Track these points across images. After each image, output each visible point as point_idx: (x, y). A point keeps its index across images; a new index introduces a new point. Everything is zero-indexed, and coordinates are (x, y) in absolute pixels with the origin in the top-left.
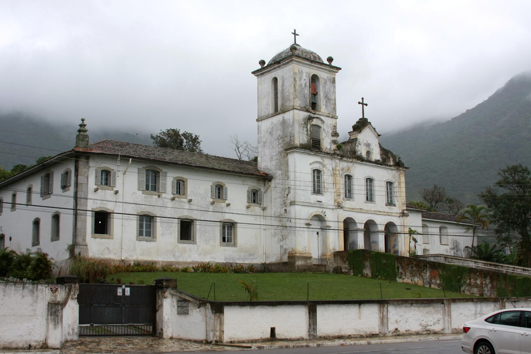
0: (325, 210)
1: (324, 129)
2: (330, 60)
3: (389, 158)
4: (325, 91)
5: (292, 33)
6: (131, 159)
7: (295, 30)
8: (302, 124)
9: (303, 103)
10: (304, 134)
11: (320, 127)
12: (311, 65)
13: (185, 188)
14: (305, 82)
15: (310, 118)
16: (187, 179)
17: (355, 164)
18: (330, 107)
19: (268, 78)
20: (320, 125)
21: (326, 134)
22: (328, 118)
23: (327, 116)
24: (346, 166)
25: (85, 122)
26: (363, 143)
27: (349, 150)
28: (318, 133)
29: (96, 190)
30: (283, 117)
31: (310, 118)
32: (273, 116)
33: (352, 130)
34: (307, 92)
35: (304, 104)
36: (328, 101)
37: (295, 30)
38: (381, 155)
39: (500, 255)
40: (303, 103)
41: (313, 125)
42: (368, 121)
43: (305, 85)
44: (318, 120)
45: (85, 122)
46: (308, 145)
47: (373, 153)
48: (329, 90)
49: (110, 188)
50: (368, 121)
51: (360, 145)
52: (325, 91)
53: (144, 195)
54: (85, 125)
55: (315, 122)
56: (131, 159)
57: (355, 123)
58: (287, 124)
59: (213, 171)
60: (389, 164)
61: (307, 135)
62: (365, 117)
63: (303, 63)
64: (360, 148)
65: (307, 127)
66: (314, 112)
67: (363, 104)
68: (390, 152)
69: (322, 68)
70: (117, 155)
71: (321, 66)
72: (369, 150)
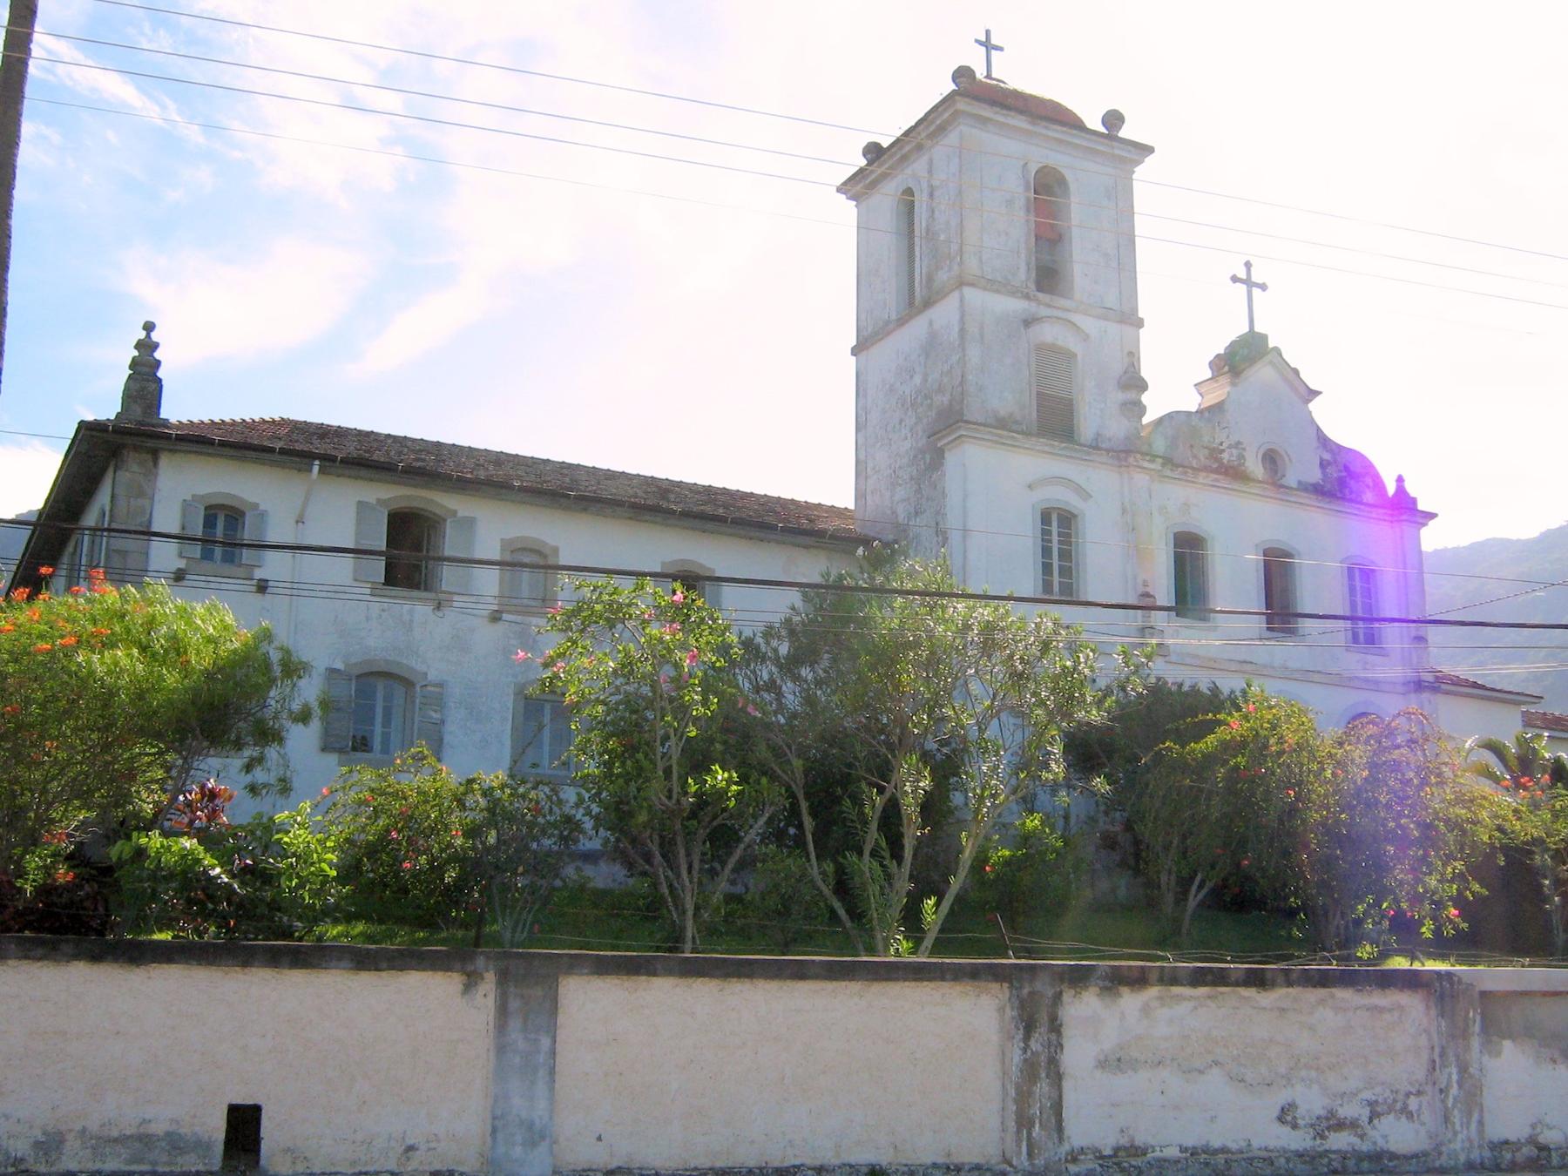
2: (1113, 119)
5: (977, 41)
7: (988, 33)
19: (890, 190)
25: (155, 336)
30: (931, 323)
32: (902, 322)
33: (1209, 374)
37: (988, 33)
42: (1271, 345)
45: (155, 336)
49: (241, 572)
50: (1271, 345)
57: (1140, 315)
58: (941, 344)
62: (1258, 329)
67: (1249, 283)
70: (280, 453)
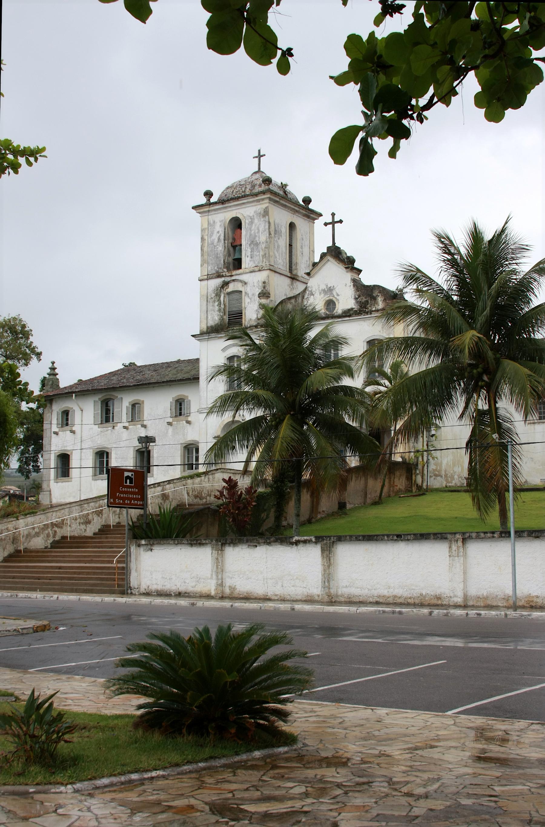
1: (246, 293)
3: (374, 299)
4: (251, 235)
6: (74, 395)
8: (212, 298)
10: (214, 311)
11: (241, 292)
13: (141, 412)
14: (218, 235)
15: (225, 284)
16: (143, 402)
20: (240, 289)
21: (251, 299)
22: (253, 274)
23: (251, 272)
26: (317, 291)
28: (240, 300)
29: (144, 426)
31: (225, 284)
35: (216, 268)
38: (356, 299)
39: (280, 459)
41: (229, 294)
43: (219, 239)
44: (236, 283)
46: (221, 325)
47: (338, 300)
48: (257, 231)
51: (313, 295)
53: (100, 429)
54: (55, 368)
55: (232, 287)
56: (74, 395)
59: (157, 385)
60: (374, 309)
61: (219, 310)
63: (215, 210)
64: (311, 300)
65: (219, 300)
66: (230, 274)
68: (379, 287)
69: (244, 203)
72: (331, 298)
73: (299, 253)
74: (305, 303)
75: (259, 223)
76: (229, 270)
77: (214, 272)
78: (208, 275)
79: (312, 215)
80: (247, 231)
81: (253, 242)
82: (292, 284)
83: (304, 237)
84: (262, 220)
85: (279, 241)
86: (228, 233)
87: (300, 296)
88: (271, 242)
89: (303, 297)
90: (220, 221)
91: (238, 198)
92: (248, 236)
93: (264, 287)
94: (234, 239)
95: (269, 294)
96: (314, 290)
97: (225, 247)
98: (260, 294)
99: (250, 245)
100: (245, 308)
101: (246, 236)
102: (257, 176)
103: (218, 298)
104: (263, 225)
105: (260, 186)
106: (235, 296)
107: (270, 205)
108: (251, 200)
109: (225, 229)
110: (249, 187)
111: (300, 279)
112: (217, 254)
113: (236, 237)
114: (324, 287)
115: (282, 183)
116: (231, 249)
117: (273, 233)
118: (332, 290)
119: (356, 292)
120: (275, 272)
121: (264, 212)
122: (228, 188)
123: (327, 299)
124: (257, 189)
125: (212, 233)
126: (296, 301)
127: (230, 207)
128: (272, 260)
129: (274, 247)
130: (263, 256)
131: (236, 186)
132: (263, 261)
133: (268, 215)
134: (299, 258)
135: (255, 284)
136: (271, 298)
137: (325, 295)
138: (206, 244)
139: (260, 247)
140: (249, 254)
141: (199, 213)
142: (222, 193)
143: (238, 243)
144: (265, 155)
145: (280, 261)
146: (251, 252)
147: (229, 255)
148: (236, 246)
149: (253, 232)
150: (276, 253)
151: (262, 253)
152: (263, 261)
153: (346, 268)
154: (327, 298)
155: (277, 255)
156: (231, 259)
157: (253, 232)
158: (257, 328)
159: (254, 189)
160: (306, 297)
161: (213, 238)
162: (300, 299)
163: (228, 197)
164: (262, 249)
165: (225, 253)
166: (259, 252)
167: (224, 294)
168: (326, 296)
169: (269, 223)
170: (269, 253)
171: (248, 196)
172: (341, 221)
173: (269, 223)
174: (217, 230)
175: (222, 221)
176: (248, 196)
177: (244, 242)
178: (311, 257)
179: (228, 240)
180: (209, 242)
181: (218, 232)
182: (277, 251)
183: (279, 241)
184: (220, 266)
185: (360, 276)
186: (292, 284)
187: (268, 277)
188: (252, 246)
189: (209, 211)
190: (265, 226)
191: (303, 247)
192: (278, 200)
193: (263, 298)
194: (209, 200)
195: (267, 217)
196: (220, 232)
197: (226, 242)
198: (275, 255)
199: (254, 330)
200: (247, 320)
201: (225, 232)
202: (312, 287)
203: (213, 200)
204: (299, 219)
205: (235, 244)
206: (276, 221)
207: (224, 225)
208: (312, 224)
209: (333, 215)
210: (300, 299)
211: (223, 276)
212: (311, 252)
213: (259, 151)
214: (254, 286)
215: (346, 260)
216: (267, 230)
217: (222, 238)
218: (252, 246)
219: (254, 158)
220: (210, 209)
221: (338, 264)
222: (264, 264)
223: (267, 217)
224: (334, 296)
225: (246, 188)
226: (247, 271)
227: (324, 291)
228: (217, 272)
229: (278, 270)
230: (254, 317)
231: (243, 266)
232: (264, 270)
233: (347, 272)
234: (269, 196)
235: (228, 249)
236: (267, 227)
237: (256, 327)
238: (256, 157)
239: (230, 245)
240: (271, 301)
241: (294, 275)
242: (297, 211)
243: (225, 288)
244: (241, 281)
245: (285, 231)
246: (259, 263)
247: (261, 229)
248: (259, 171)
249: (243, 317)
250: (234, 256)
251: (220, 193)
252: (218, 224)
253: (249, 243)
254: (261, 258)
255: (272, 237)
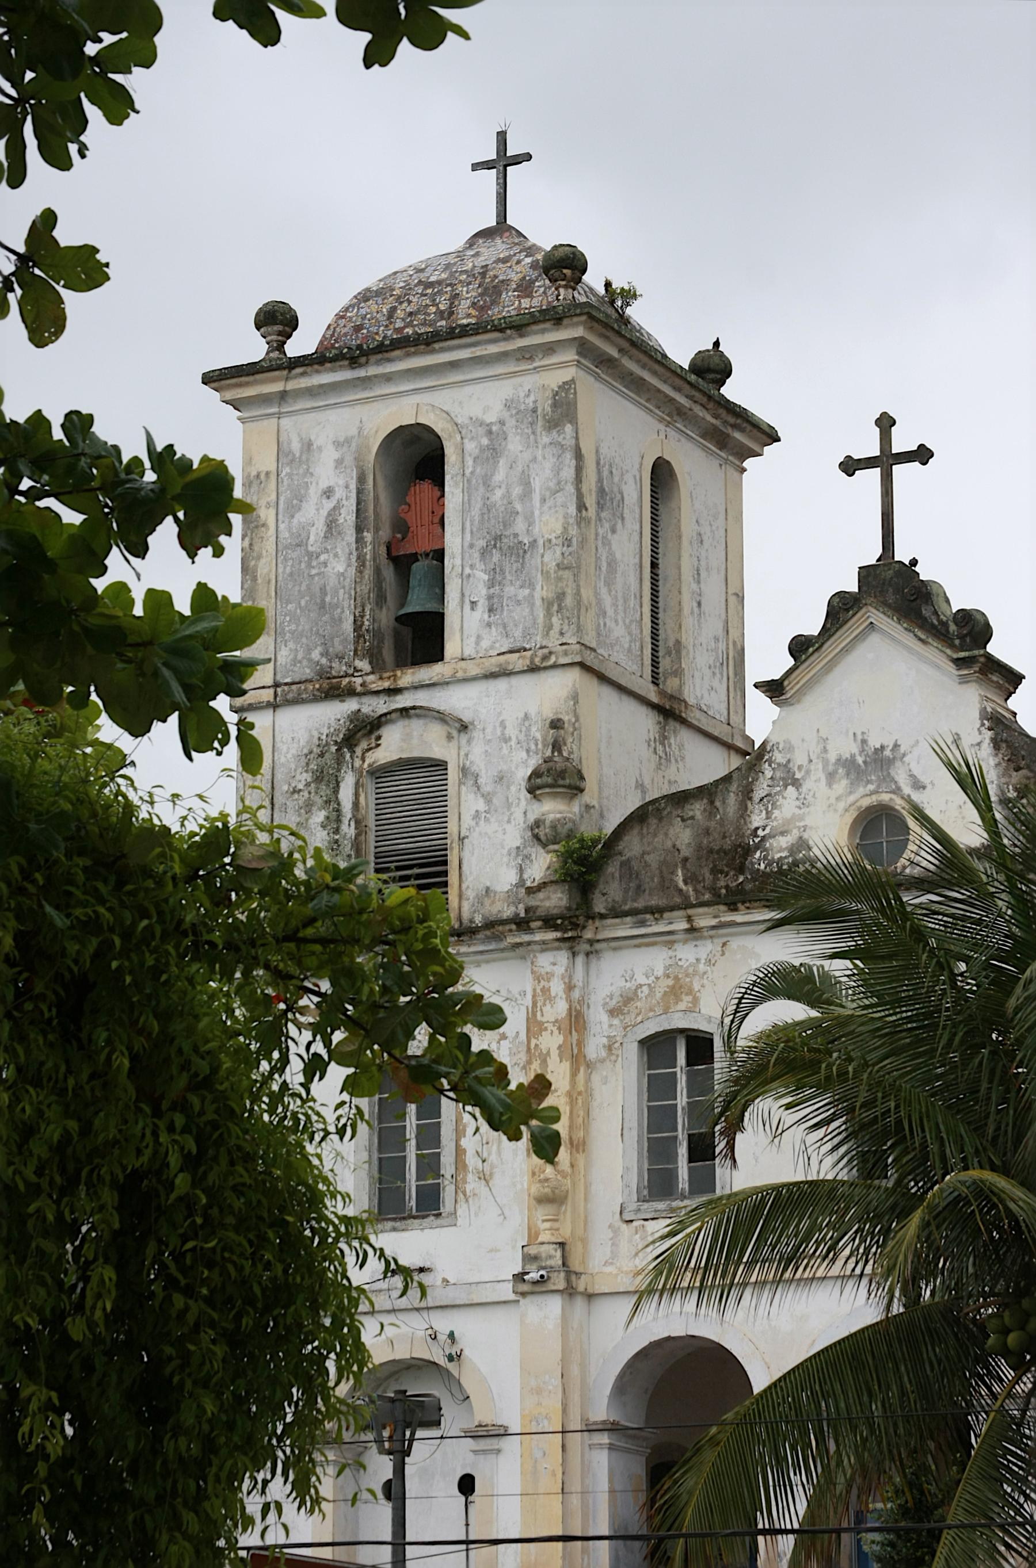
0: (443, 1323)
1: (464, 771)
4: (488, 507)
8: (296, 791)
9: (309, 650)
11: (439, 766)
12: (365, 382)
14: (329, 505)
17: (735, 943)
18: (530, 600)
21: (488, 798)
22: (502, 684)
23: (491, 675)
24: (659, 971)
26: (817, 767)
27: (686, 852)
34: (341, 568)
35: (316, 655)
36: (510, 567)
40: (309, 650)
41: (381, 773)
43: (332, 524)
44: (416, 725)
48: (517, 491)
51: (796, 783)
52: (488, 507)
63: (311, 392)
64: (788, 804)
65: (332, 801)
66: (386, 684)
69: (454, 365)
71: (433, 351)
72: (885, 797)
73: (688, 604)
74: (757, 820)
75: (527, 456)
76: (378, 667)
77: (308, 673)
78: (276, 685)
79: (737, 435)
80: (468, 490)
81: (498, 538)
82: (663, 739)
83: (706, 530)
84: (546, 440)
85: (614, 539)
86: (376, 498)
87: (734, 787)
88: (583, 542)
89: (747, 793)
90: (337, 444)
91: (427, 341)
92: (476, 512)
93: (557, 746)
94: (401, 527)
95: (582, 778)
96: (799, 758)
97: (361, 559)
98: (536, 774)
99: (484, 553)
100: (461, 839)
101: (465, 509)
102: (499, 247)
103: (325, 790)
104: (548, 464)
105: (525, 288)
106: (403, 785)
107: (581, 373)
108: (493, 349)
109: (361, 479)
110: (469, 294)
111: (694, 716)
112: (323, 591)
113: (411, 519)
114: (848, 748)
115: (608, 285)
116: (389, 573)
117: (590, 501)
118: (890, 762)
119: (1006, 773)
120: (603, 678)
121: (555, 405)
122: (365, 296)
123: (866, 802)
124: (510, 305)
125: (299, 498)
126: (712, 811)
127: (388, 378)
128: (589, 620)
129: (598, 568)
130: (548, 604)
131: (408, 289)
132: (549, 627)
133: (573, 420)
134: (689, 622)
135: (512, 732)
136: (587, 798)
137: (853, 785)
138: (270, 546)
139: (534, 561)
140: (479, 591)
141: (236, 404)
142: (340, 317)
143: (423, 545)
144: (528, 157)
145: (619, 631)
146: (491, 583)
147: (381, 599)
148: (414, 558)
149: (499, 493)
150: (604, 591)
151: (541, 591)
152: (549, 627)
153: (959, 663)
154: (864, 796)
155: (607, 601)
156: (386, 618)
157: (499, 493)
158: (529, 930)
159: (494, 302)
160: (759, 793)
161: (300, 518)
162: (732, 799)
163: (370, 337)
164: (546, 574)
165: (365, 588)
166: (532, 586)
167: (359, 773)
168: (861, 791)
169: (579, 455)
170: (578, 593)
171: (465, 332)
172: (922, 455)
173: (579, 455)
174: (324, 485)
175: (348, 441)
176: (465, 332)
177: (453, 541)
178: (733, 622)
179: (377, 529)
180: (285, 534)
181: (328, 493)
182: (609, 584)
183: (614, 539)
184: (338, 647)
185: (1013, 703)
186: (663, 739)
187: (575, 697)
188: (496, 556)
189: (283, 396)
190: (557, 470)
191: (703, 574)
192: (614, 353)
193: (555, 795)
194: (280, 347)
195: (569, 428)
196: (339, 493)
197: (368, 536)
198: (599, 602)
199: (511, 940)
200: (470, 894)
201: (360, 492)
202: (790, 748)
203: (297, 347)
204: (688, 446)
205: (408, 549)
206: (603, 451)
207: (359, 460)
208: (732, 473)
209: (886, 423)
210: (732, 799)
211: (351, 692)
212: (732, 600)
213: (502, 138)
214: (506, 740)
215: (953, 627)
216: (570, 489)
217: (348, 517)
218: (496, 556)
219: (476, 167)
220: (291, 385)
221: (918, 646)
222: (553, 642)
223: (569, 428)
224: (897, 791)
225: (455, 296)
226: (473, 670)
227: (849, 765)
228: (324, 674)
229: (613, 674)
230: (506, 879)
231: (452, 647)
232: (555, 666)
233: (964, 680)
234: (579, 332)
235: (378, 571)
236: (568, 473)
237: (522, 924)
238: (488, 165)
239: (383, 550)
240: (588, 807)
241: (672, 697)
242: (680, 412)
243: (364, 745)
244: (441, 717)
245: (635, 495)
246: (527, 634)
247: (537, 484)
248: (501, 227)
249: (453, 878)
250: (403, 602)
251: (329, 318)
252: (329, 456)
253: (482, 543)
254: (540, 614)
255: (588, 521)
